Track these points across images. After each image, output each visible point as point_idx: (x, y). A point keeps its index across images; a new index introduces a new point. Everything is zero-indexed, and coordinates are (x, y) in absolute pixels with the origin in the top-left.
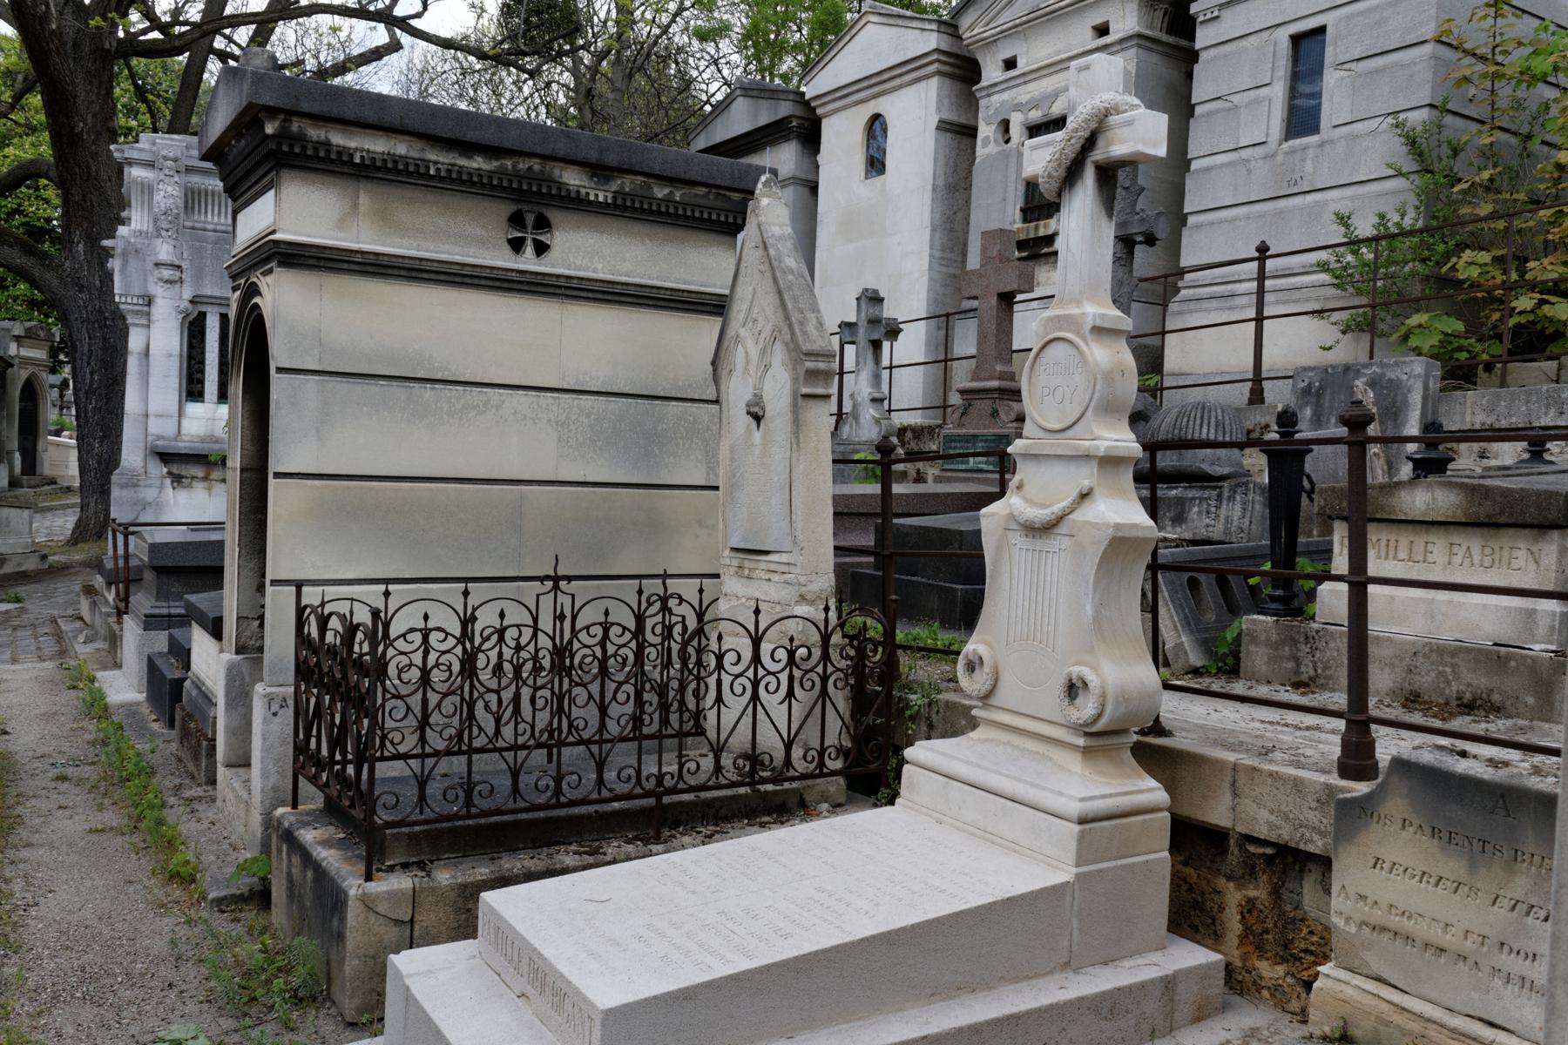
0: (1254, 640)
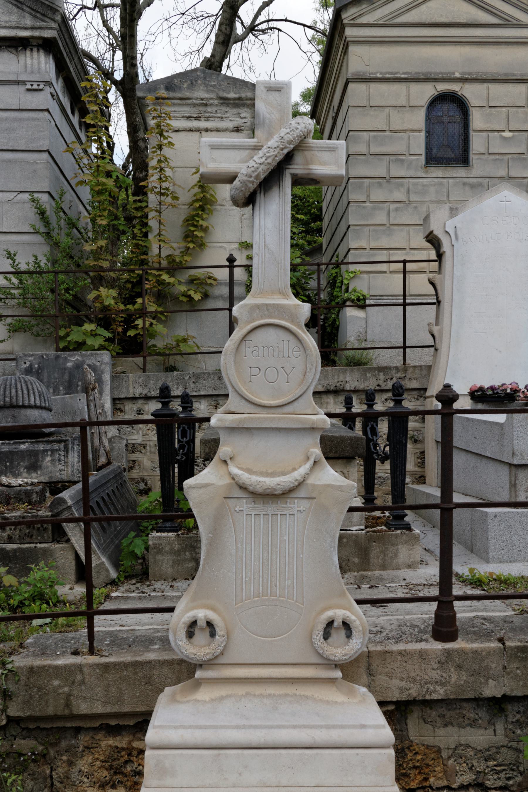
0: (159, 551)
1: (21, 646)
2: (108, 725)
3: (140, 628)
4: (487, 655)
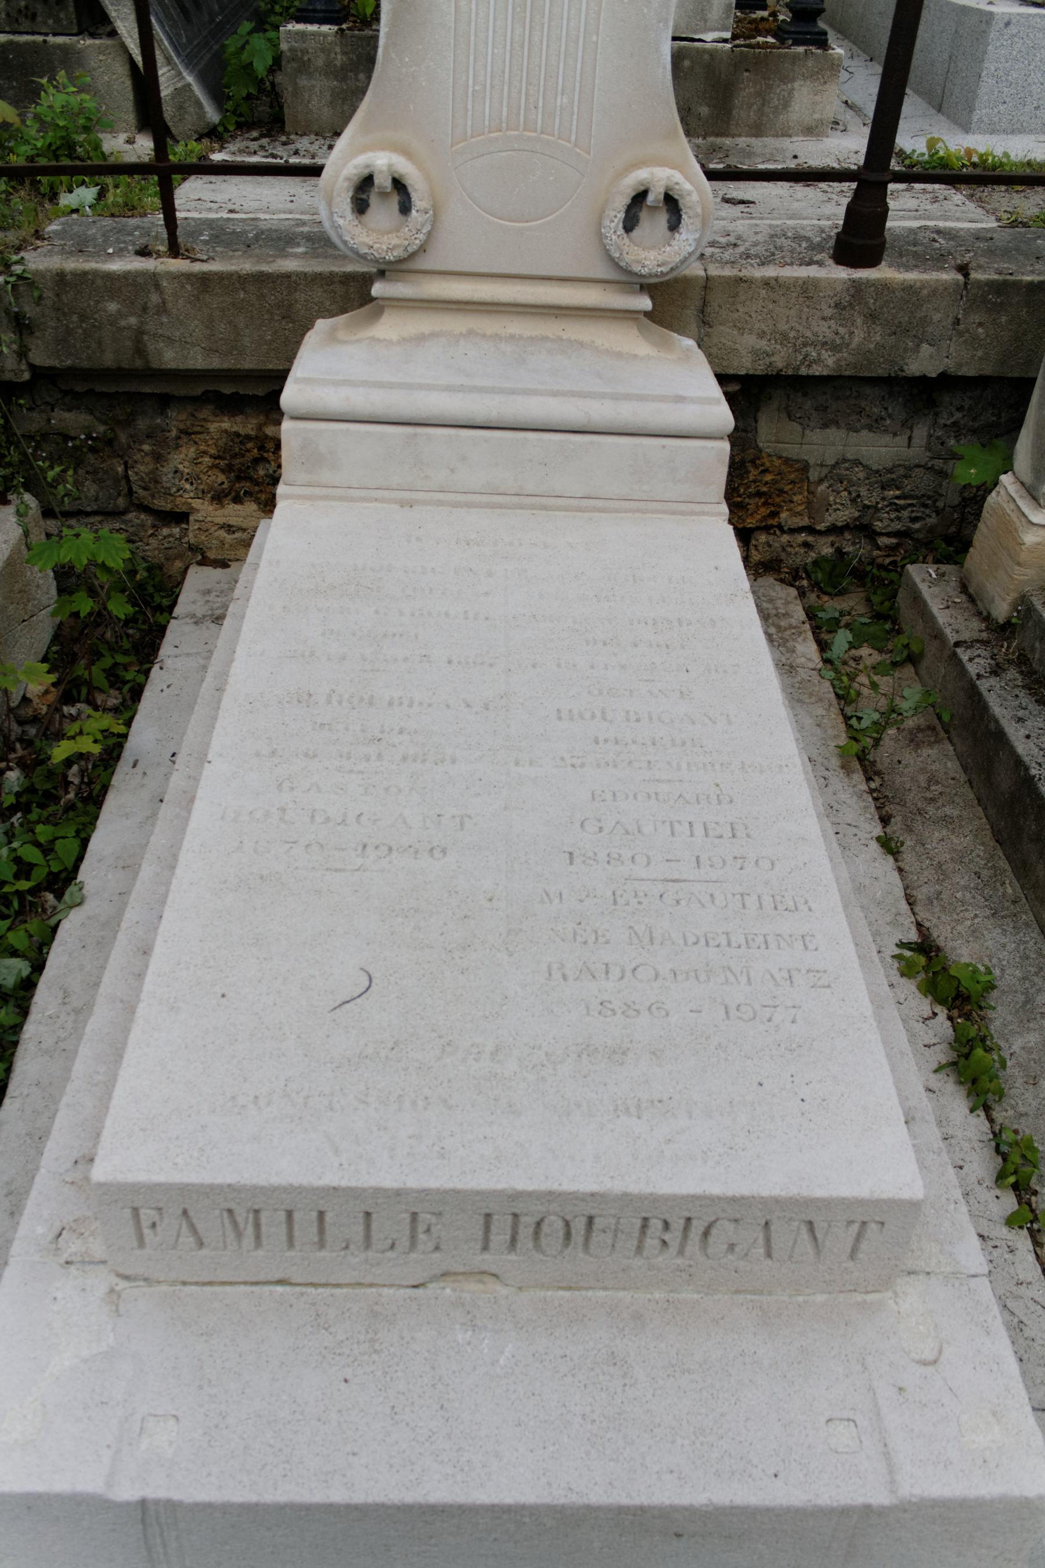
0: (304, 67)
1: (38, 235)
2: (217, 393)
3: (267, 217)
4: (929, 296)
